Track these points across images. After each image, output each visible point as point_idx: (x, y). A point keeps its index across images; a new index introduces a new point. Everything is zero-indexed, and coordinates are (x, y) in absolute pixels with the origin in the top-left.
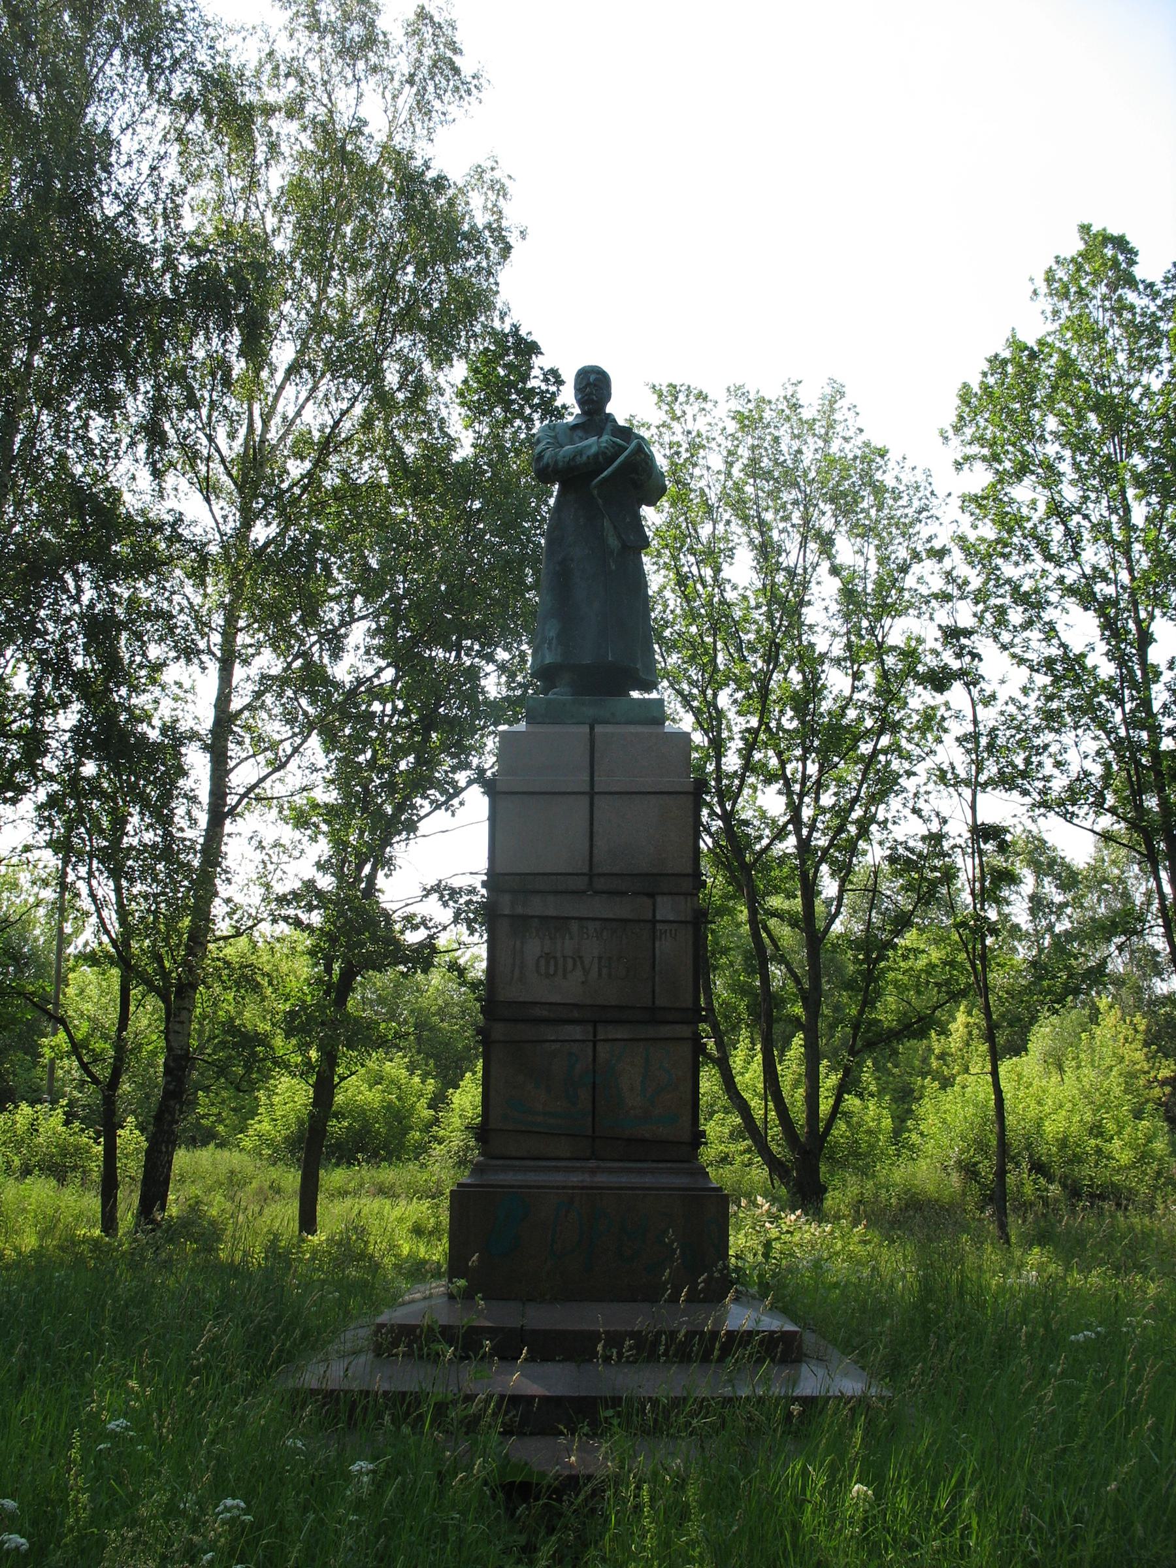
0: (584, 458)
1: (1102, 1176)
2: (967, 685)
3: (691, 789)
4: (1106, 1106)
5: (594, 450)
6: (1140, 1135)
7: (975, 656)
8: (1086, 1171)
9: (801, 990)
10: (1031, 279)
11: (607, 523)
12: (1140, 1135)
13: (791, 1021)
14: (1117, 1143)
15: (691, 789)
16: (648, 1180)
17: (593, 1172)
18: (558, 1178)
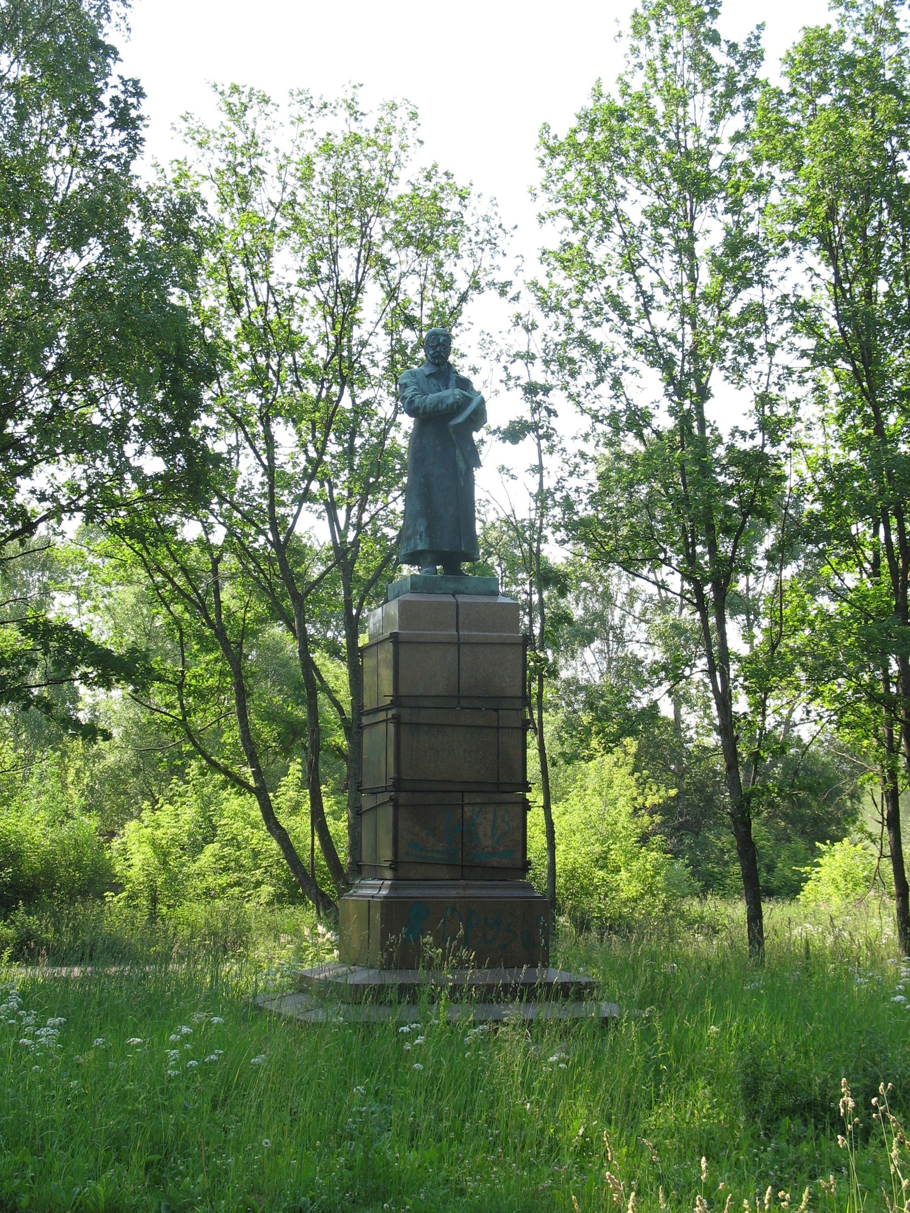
0: (444, 406)
1: (611, 908)
2: (540, 438)
3: (521, 641)
4: (613, 835)
5: (451, 400)
6: (648, 866)
7: (551, 412)
8: (593, 903)
9: (344, 720)
10: (617, 21)
11: (458, 452)
12: (648, 866)
13: (333, 752)
14: (624, 874)
15: (521, 641)
16: (498, 893)
17: (464, 888)
18: (443, 893)
